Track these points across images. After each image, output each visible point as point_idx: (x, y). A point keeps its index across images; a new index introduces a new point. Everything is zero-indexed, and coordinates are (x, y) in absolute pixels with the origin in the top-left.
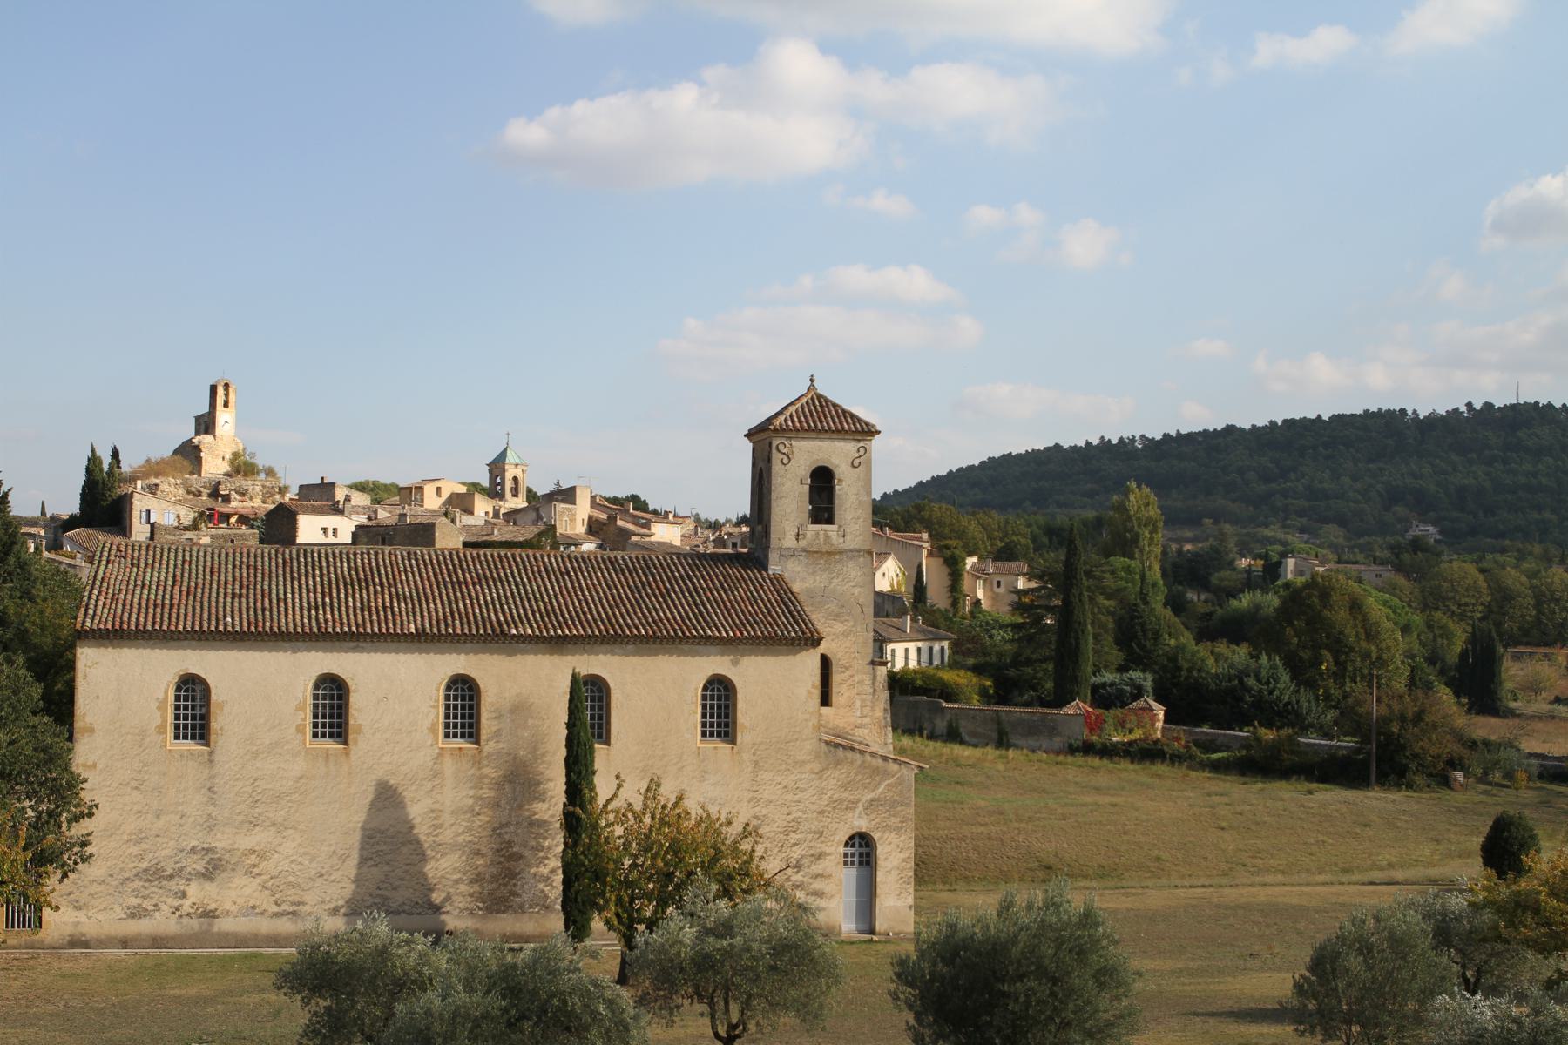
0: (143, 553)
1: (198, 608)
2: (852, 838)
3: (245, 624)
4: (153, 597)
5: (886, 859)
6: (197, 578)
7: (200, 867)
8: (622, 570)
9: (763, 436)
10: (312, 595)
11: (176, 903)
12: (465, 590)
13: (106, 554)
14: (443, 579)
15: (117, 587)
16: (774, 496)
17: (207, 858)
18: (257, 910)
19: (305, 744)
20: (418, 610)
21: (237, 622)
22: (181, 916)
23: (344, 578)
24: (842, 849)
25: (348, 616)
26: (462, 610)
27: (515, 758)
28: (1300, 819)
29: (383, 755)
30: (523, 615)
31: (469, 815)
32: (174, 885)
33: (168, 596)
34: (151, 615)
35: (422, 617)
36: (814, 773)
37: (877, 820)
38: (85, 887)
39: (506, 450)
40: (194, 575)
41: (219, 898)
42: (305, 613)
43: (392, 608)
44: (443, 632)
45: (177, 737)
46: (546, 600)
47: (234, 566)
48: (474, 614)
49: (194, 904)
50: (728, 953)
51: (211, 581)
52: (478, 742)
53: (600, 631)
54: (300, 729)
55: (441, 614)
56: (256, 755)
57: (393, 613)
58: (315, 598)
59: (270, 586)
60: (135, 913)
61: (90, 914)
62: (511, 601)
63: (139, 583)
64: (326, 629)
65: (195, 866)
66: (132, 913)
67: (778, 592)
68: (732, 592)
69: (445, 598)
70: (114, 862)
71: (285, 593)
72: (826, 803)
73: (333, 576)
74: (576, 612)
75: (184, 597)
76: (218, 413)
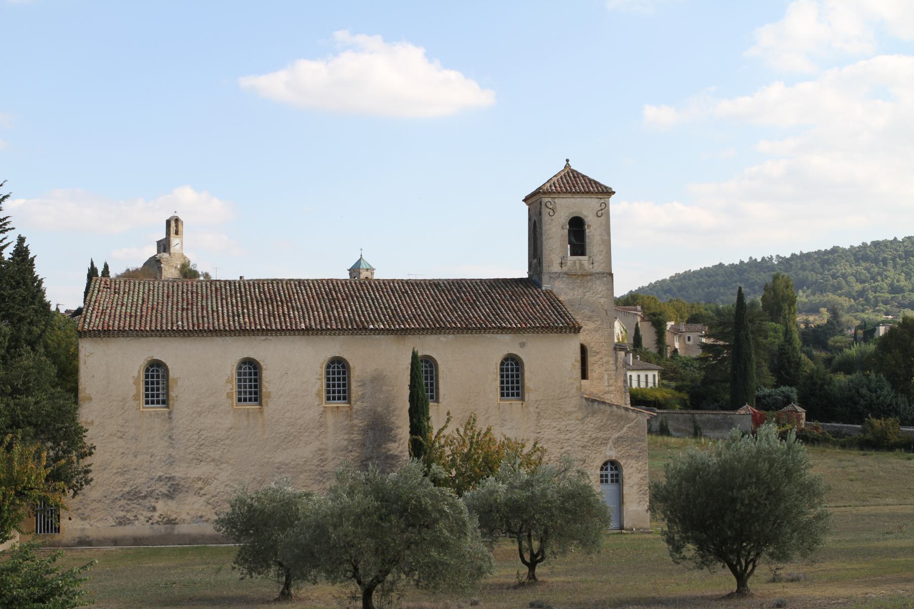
0: (122, 285)
1: (159, 317)
2: (605, 464)
3: (191, 325)
4: (129, 311)
5: (629, 478)
6: (158, 300)
7: (164, 490)
8: (443, 290)
9: (535, 200)
10: (235, 308)
11: (149, 514)
12: (337, 303)
13: (97, 286)
14: (323, 297)
15: (105, 305)
16: (544, 237)
17: (169, 484)
18: (203, 519)
19: (233, 406)
20: (306, 315)
21: (185, 324)
22: (152, 524)
23: (256, 297)
24: (599, 472)
25: (259, 319)
26: (336, 315)
27: (375, 413)
28: (905, 474)
29: (286, 412)
30: (377, 317)
31: (344, 452)
32: (146, 503)
33: (139, 310)
34: (128, 322)
35: (310, 319)
36: (578, 420)
37: (623, 451)
38: (88, 505)
39: (360, 260)
40: (156, 298)
41: (178, 511)
42: (231, 318)
43: (289, 314)
44: (324, 327)
45: (147, 403)
46: (393, 308)
47: (183, 292)
48: (344, 317)
49: (161, 515)
50: (532, 498)
51: (168, 301)
52: (349, 402)
53: (429, 325)
54: (229, 396)
55: (322, 317)
56: (200, 414)
57: (290, 317)
58: (238, 310)
59: (207, 304)
60: (122, 522)
61: (92, 523)
62: (369, 309)
63: (120, 303)
64: (245, 327)
65: (161, 489)
66: (120, 522)
67: (549, 300)
68: (518, 301)
69: (324, 308)
70: (108, 487)
71: (217, 307)
72: (587, 440)
73: (249, 296)
74: (413, 315)
75: (150, 311)
76: (172, 238)
